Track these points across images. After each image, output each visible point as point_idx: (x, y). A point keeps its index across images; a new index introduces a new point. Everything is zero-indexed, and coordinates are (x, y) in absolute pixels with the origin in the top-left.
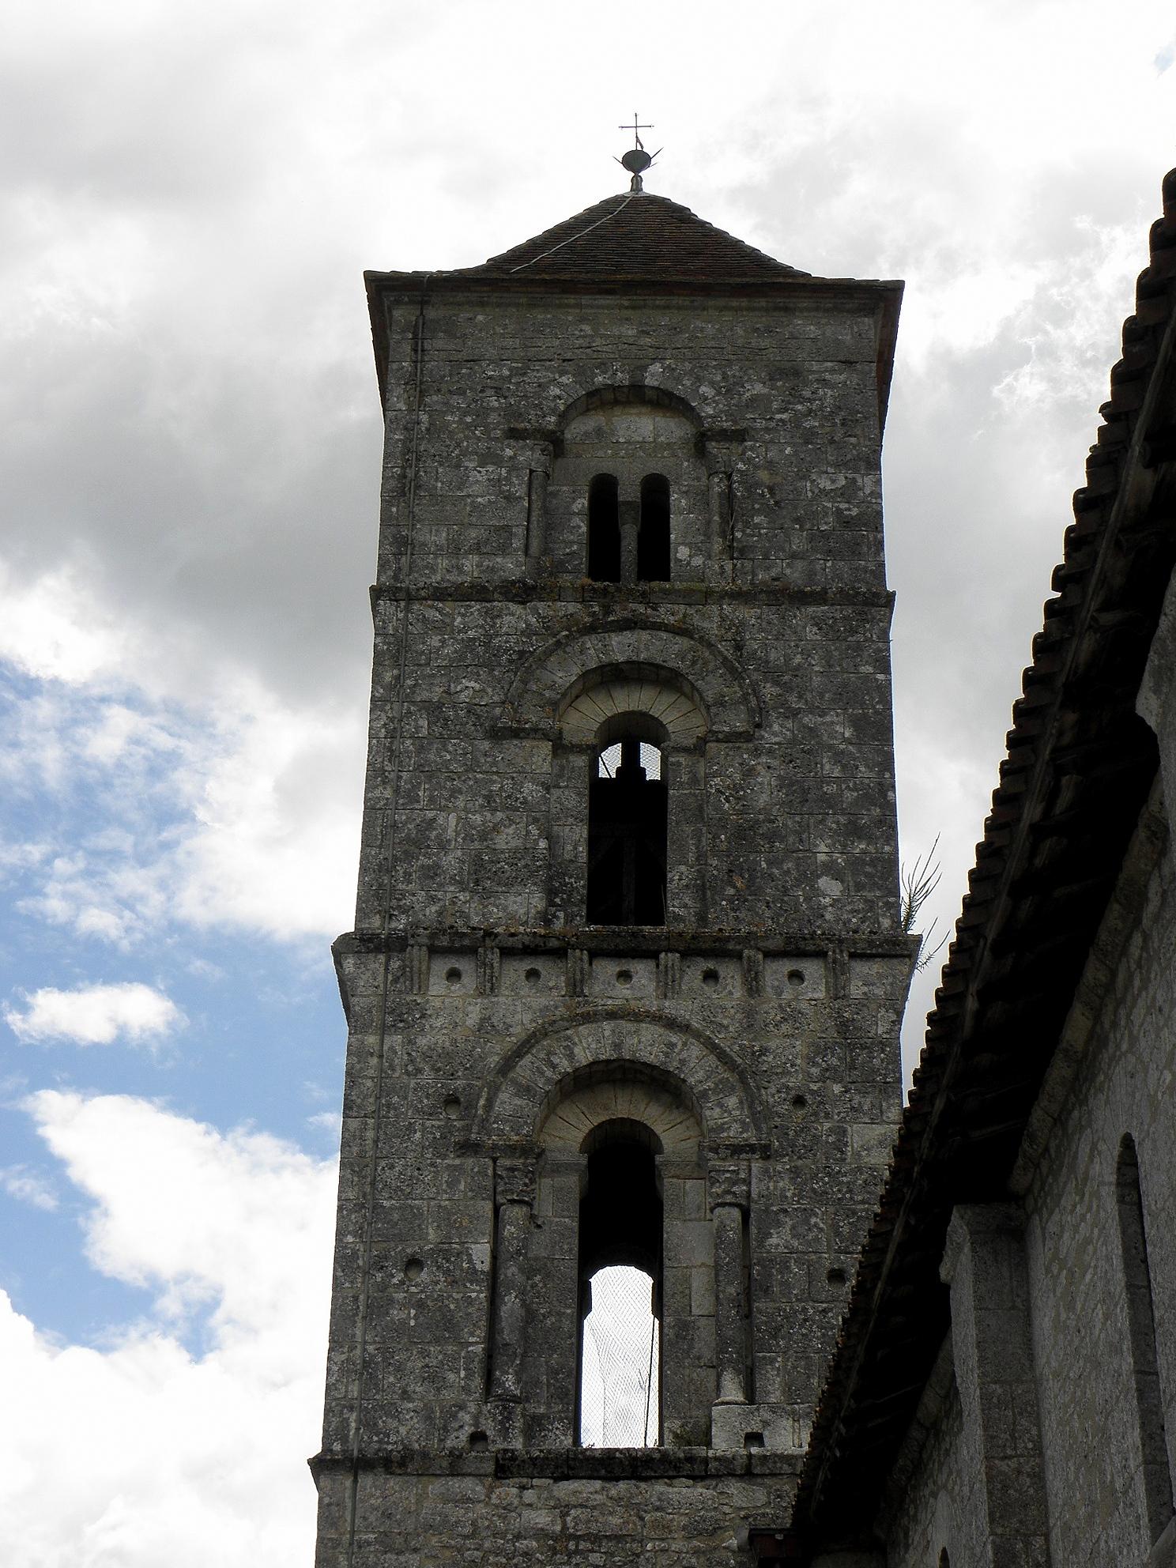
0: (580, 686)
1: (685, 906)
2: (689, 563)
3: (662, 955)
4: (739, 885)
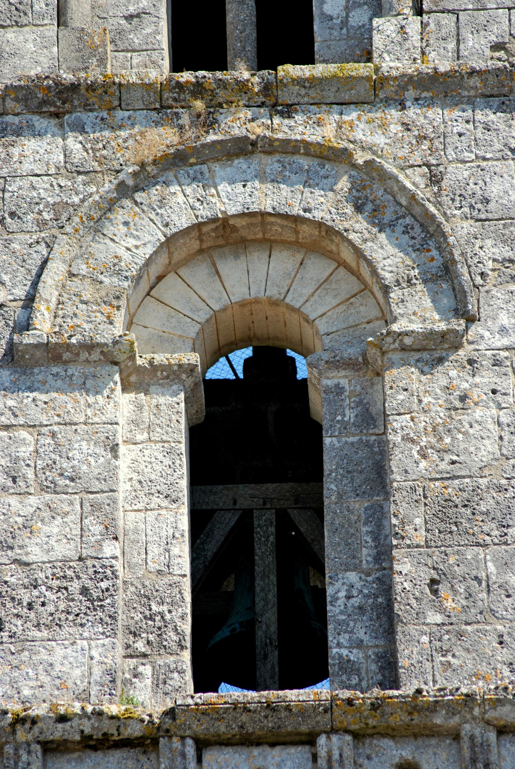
0: (163, 260)
1: (359, 644)
2: (345, 23)
3: (322, 740)
4: (449, 604)
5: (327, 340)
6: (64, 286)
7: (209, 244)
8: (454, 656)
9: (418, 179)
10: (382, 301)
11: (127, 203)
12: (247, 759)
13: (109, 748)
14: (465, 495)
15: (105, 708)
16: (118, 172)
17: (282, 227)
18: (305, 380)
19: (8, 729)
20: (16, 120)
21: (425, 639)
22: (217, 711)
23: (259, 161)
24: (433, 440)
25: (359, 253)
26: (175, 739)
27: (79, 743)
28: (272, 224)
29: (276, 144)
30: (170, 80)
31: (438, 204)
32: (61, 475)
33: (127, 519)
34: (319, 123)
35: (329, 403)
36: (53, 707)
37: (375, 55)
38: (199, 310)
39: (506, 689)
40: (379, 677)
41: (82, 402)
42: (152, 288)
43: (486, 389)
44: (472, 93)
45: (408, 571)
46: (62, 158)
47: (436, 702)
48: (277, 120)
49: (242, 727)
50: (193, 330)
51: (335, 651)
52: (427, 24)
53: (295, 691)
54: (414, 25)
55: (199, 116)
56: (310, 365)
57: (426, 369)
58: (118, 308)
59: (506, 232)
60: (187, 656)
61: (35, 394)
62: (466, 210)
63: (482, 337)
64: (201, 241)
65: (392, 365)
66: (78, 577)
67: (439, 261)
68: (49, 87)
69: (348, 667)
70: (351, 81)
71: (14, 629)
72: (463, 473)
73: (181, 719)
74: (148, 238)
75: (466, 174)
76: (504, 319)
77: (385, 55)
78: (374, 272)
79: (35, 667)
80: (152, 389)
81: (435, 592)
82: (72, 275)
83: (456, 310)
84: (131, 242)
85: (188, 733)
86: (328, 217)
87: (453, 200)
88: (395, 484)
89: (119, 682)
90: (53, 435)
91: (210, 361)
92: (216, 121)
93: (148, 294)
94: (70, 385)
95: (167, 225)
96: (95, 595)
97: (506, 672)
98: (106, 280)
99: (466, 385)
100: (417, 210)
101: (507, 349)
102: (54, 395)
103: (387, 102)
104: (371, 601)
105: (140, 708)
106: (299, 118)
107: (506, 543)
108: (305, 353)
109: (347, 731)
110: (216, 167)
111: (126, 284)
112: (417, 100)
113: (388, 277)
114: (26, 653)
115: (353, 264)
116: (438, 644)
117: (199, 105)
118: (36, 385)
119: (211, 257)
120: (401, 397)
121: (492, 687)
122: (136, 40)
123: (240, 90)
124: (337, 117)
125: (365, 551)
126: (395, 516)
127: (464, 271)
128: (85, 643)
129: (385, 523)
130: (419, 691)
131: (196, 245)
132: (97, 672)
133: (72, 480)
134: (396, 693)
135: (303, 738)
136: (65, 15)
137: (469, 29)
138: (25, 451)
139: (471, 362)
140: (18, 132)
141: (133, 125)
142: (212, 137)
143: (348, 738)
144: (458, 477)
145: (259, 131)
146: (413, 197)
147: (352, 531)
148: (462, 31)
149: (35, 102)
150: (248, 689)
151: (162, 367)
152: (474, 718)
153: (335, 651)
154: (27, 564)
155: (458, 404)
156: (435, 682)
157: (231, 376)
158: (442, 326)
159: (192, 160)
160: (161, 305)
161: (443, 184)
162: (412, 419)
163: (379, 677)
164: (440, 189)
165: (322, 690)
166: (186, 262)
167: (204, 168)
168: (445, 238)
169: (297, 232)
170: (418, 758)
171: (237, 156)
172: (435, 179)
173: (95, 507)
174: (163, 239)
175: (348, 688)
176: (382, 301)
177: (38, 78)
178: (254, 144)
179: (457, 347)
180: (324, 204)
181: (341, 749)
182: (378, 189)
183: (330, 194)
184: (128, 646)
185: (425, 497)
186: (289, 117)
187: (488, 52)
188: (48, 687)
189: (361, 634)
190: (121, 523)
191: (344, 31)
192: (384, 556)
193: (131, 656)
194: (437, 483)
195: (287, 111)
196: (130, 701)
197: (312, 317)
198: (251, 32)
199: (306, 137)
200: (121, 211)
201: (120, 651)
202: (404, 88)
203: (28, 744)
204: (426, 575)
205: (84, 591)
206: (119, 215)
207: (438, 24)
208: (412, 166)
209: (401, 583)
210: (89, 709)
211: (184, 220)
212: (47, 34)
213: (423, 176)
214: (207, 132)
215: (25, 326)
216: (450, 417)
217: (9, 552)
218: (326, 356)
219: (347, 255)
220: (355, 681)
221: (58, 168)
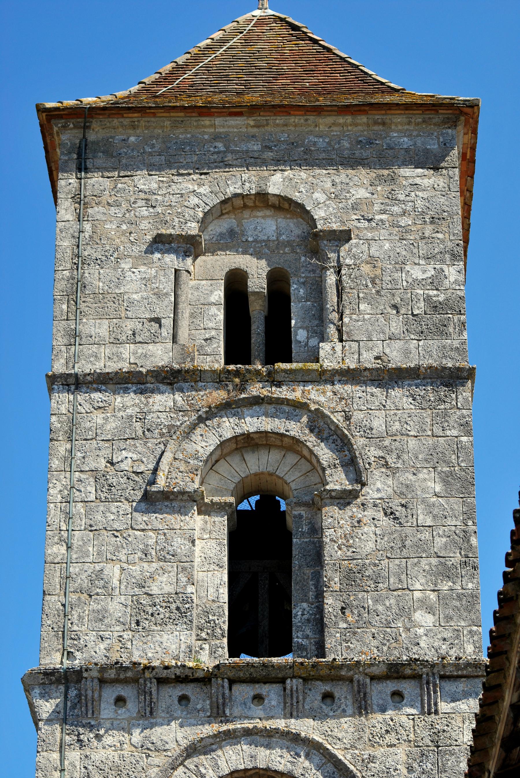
0: (218, 452)
1: (307, 637)
2: (307, 344)
3: (288, 681)
4: (350, 619)
5: (295, 492)
6: (171, 464)
7: (241, 446)
8: (351, 643)
9: (340, 418)
10: (321, 475)
11: (202, 425)
12: (253, 689)
13: (188, 682)
14: (359, 567)
15: (186, 664)
16: (199, 411)
17: (275, 438)
18: (284, 511)
19: (141, 672)
20: (152, 386)
21: (338, 635)
22: (239, 666)
23: (264, 407)
24: (345, 541)
25: (311, 452)
26: (219, 679)
27: (174, 679)
28: (271, 437)
29: (273, 399)
30: (224, 368)
31: (349, 430)
32: (168, 553)
33: (199, 575)
34: (294, 390)
35: (296, 523)
36: (162, 662)
37: (320, 360)
38: (235, 477)
39: (375, 659)
40: (316, 652)
41: (179, 519)
42: (213, 466)
43: (369, 518)
44: (365, 379)
45: (331, 603)
46: (172, 404)
47: (342, 664)
48: (274, 388)
49: (251, 674)
50: (232, 486)
51: (295, 640)
52: (345, 346)
53: (276, 658)
54: (339, 346)
55: (237, 385)
56: (287, 504)
57: (342, 507)
58: (197, 475)
59: (381, 444)
60: (225, 640)
61: (157, 515)
62: (362, 433)
63: (368, 493)
64: (237, 444)
65: (326, 505)
66: (175, 602)
67: (349, 457)
68: (167, 371)
69: (301, 647)
70: (309, 371)
71: (145, 625)
72: (358, 557)
73: (222, 670)
74: (212, 442)
75: (362, 416)
76: (379, 485)
77: (325, 360)
78: (318, 461)
79: (154, 643)
80: (212, 514)
81: (343, 613)
82: (175, 459)
83: (356, 480)
84: (204, 444)
85: (225, 676)
86: (297, 434)
87: (356, 428)
88: (326, 562)
89: (193, 652)
90: (165, 534)
91: (239, 501)
92: (245, 388)
93: (211, 469)
94: (173, 511)
95: (221, 436)
96: (183, 611)
97: (376, 651)
98: (192, 462)
99: (360, 516)
100: (339, 432)
101: (380, 499)
102: (166, 515)
103: (326, 382)
104: (313, 617)
105: (203, 664)
106: (284, 388)
107: (377, 591)
108: (285, 498)
109: (300, 677)
110: (245, 410)
111: (201, 464)
112: (340, 381)
113: (325, 464)
114: (150, 637)
115: (309, 457)
116: (344, 637)
117: (237, 380)
118: (157, 510)
119: (241, 452)
120: (330, 521)
121: (369, 658)
122: (209, 350)
123: (257, 374)
124: (302, 388)
125: (311, 593)
126: (326, 577)
127: (361, 461)
128: (178, 633)
129: (321, 580)
130: (334, 659)
131: (234, 446)
132: (183, 647)
133: (173, 556)
134: (324, 660)
135: (280, 680)
136: (176, 338)
137: (364, 349)
138: (151, 542)
139: (363, 505)
140: (152, 392)
141: (206, 390)
142: (243, 396)
143: (301, 680)
144: (356, 559)
145: (265, 393)
146: (337, 426)
147: (305, 583)
148: (361, 350)
149: (161, 378)
150: (254, 657)
151: (217, 504)
152: (360, 672)
153: (295, 640)
154: (151, 595)
155: (356, 524)
156: (342, 655)
157: (250, 509)
158: (350, 487)
159: (234, 406)
160: (217, 474)
161: (351, 420)
162: (335, 531)
163: (316, 652)
164: (350, 423)
165: (289, 658)
166: (230, 453)
167: (239, 410)
168: (352, 446)
169: (282, 441)
170: (333, 690)
171: (255, 404)
172: (347, 418)
173: (184, 569)
174: (219, 443)
175: (301, 657)
176: (321, 475)
177: (163, 366)
178: (263, 399)
179: (357, 497)
180: (295, 428)
181: (297, 685)
182: (321, 422)
183: (298, 424)
184: (198, 635)
185: (340, 568)
186: (280, 387)
187: (373, 360)
188: (160, 653)
189: (308, 632)
190: (195, 577)
191: (306, 348)
192: (320, 596)
193: (199, 640)
194: (346, 562)
195: (279, 385)
196: (198, 661)
197: (288, 482)
198: (263, 348)
199: (287, 397)
200: (199, 429)
201: (194, 637)
202: (334, 375)
203: (150, 679)
204: (339, 605)
205: (178, 609)
206: (198, 431)
207: (350, 346)
208: (337, 412)
209: (328, 609)
210: (179, 664)
211: (229, 434)
212: (168, 347)
213: (342, 416)
214: (241, 393)
215: (152, 482)
216: (353, 530)
217: (143, 589)
218: (294, 500)
219: (306, 452)
220: (304, 654)
221: (170, 409)
